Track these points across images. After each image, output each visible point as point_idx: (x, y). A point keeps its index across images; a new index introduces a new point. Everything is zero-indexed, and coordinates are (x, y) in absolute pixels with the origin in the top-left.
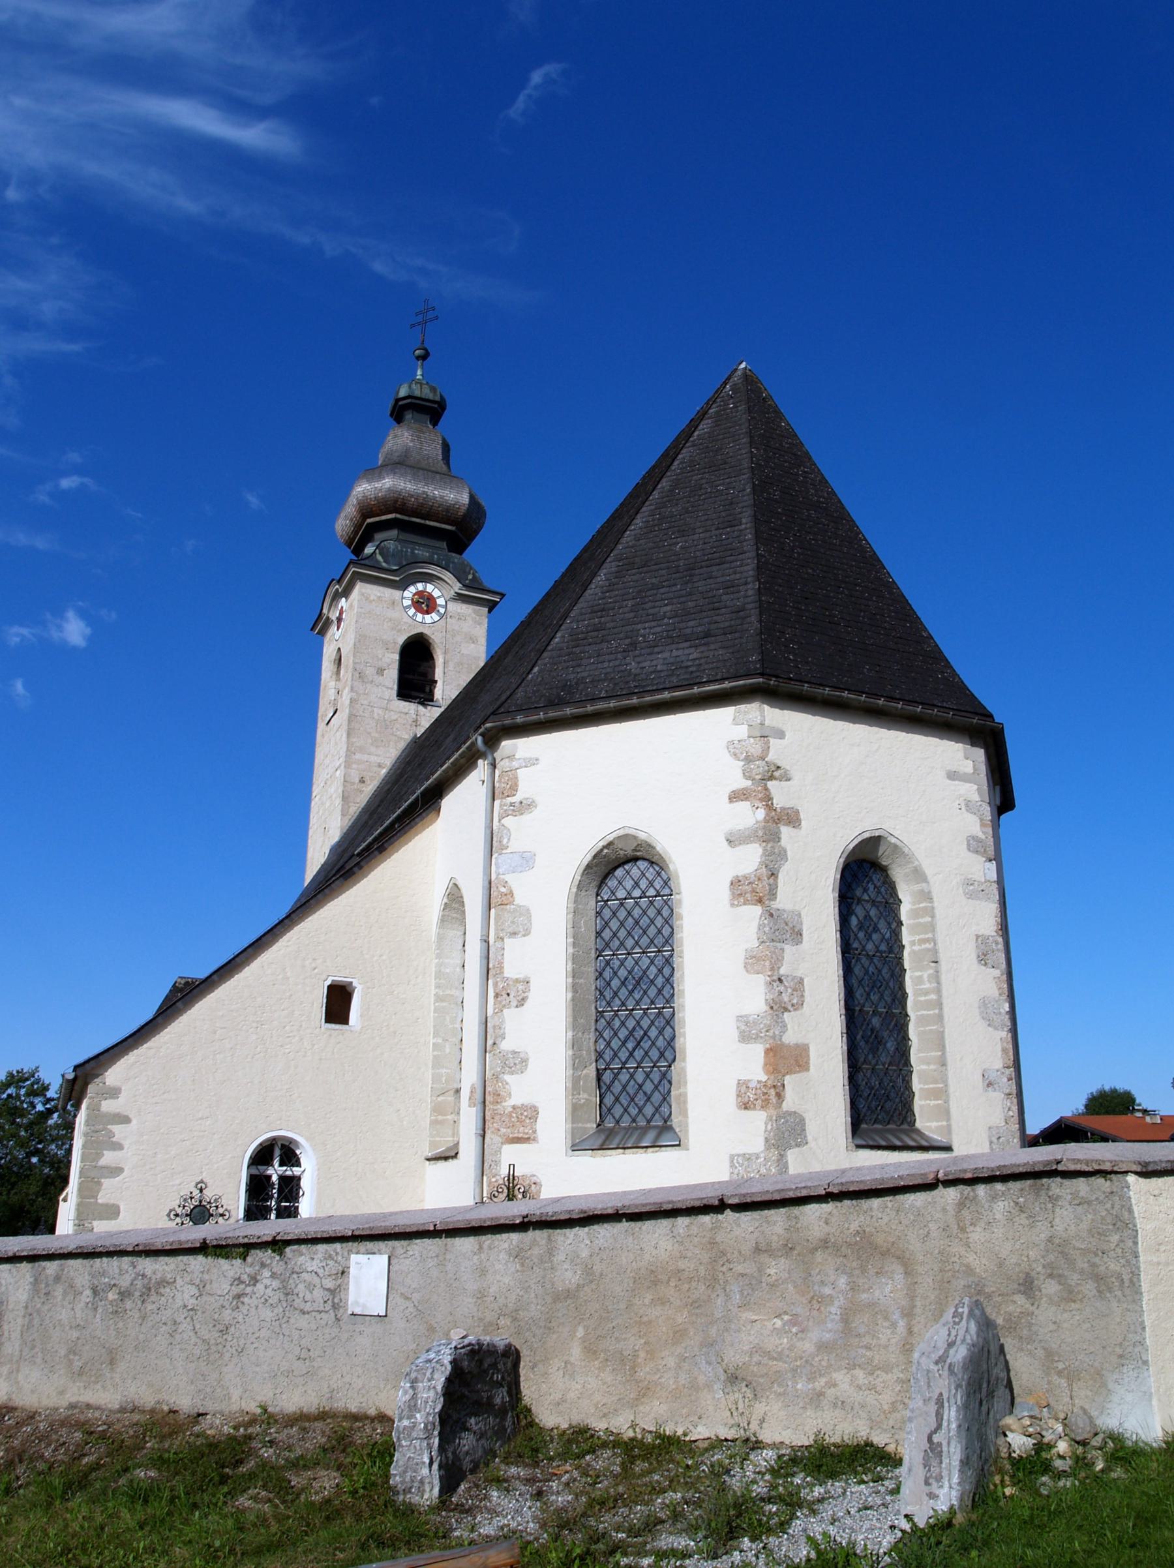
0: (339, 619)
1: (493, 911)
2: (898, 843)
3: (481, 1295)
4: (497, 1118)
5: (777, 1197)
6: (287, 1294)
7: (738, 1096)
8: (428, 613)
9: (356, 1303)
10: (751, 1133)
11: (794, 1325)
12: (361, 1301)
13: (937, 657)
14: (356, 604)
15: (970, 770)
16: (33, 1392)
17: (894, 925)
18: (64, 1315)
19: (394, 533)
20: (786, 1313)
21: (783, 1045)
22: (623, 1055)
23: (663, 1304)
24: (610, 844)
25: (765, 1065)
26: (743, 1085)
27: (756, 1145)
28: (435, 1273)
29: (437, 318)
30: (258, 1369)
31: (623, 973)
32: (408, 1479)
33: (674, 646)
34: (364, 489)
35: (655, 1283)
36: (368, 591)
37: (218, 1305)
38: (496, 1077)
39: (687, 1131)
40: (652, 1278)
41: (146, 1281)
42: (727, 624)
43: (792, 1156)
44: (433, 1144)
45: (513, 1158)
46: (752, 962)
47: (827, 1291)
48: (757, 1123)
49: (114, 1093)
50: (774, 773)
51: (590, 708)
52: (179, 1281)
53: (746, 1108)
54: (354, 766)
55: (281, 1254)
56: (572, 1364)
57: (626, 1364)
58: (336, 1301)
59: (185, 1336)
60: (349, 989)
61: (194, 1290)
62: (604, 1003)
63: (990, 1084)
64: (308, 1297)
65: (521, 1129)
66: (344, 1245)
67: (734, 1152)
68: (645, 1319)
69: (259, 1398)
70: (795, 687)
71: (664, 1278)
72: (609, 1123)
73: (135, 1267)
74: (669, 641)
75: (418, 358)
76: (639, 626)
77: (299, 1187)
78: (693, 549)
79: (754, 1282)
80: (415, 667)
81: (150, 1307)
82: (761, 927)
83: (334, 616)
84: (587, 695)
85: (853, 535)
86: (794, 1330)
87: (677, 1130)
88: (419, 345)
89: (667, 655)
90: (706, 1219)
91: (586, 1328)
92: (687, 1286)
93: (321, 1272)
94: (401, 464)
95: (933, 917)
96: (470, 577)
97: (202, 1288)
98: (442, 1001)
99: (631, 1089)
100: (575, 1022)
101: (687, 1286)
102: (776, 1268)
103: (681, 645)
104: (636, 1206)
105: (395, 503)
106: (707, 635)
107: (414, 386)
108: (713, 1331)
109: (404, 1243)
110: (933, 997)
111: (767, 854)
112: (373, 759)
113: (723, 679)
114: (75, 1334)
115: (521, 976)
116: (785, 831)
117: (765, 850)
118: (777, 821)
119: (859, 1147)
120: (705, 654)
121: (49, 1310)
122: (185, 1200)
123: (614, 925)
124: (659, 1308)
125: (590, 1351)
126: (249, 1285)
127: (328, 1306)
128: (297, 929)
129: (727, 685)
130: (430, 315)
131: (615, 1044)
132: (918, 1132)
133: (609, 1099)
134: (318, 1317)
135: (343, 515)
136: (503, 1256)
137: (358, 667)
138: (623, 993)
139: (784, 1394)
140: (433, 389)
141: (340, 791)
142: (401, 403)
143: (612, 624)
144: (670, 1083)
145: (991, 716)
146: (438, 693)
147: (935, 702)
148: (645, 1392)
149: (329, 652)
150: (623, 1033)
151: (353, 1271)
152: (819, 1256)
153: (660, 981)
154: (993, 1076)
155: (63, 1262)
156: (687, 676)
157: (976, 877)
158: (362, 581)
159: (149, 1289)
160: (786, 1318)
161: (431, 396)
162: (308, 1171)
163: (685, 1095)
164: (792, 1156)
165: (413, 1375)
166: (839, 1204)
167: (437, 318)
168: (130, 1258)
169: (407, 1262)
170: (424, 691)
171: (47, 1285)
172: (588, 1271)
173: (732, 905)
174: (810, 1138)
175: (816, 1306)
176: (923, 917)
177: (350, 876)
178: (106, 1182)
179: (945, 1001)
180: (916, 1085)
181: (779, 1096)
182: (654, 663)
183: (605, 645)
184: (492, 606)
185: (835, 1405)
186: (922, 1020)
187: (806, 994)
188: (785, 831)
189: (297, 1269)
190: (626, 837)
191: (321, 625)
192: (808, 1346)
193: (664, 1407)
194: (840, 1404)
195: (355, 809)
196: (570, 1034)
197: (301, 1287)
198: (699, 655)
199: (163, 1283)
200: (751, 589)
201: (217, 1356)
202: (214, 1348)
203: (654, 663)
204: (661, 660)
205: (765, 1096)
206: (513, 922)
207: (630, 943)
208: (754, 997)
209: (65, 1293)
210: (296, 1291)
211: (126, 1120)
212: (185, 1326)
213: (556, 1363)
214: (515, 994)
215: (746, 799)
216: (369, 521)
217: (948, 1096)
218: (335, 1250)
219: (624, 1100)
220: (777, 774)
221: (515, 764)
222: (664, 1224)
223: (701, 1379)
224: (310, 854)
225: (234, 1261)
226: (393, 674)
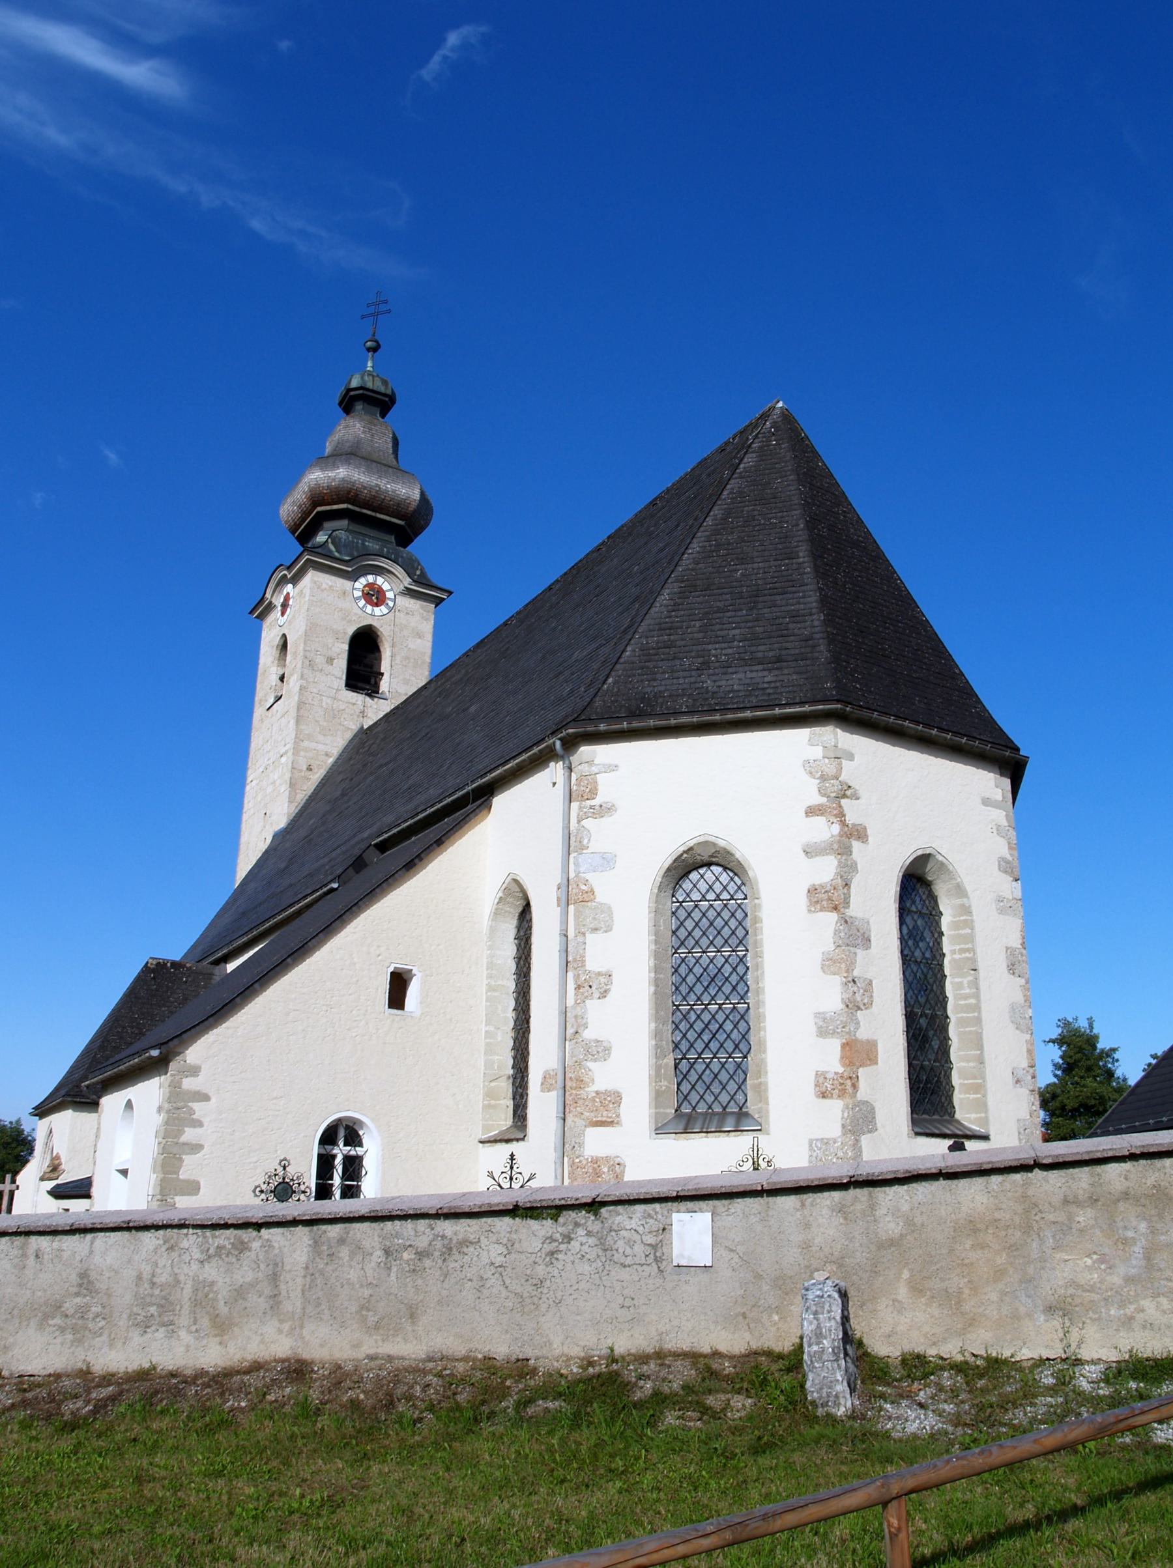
0: (285, 606)
1: (571, 907)
2: (944, 861)
3: (806, 1246)
4: (581, 1102)
5: (1087, 1157)
6: (606, 1250)
7: (816, 1085)
8: (377, 605)
9: (682, 1256)
10: (830, 1118)
11: (1102, 1263)
12: (686, 1254)
13: (968, 692)
14: (307, 592)
15: (999, 797)
16: (322, 1346)
17: (936, 935)
18: (353, 1275)
19: (344, 523)
20: (1095, 1253)
21: (856, 1040)
22: (699, 1046)
23: (982, 1248)
24: (691, 849)
25: (842, 1058)
26: (821, 1076)
27: (834, 1130)
28: (759, 1228)
29: (389, 311)
30: (578, 1318)
31: (698, 970)
32: (824, 1395)
33: (747, 668)
34: (316, 477)
35: (975, 1231)
36: (321, 579)
37: (531, 1261)
38: (579, 1063)
39: (767, 1118)
40: (971, 1227)
41: (446, 1242)
42: (797, 651)
43: (865, 1140)
44: (486, 1128)
45: (596, 1143)
46: (829, 964)
47: (1130, 1234)
48: (835, 1109)
49: (194, 1071)
50: (846, 792)
51: (673, 722)
52: (484, 1241)
53: (824, 1097)
54: (302, 753)
55: (596, 1215)
56: (899, 1302)
57: (952, 1300)
58: (658, 1254)
59: (494, 1290)
60: (405, 977)
61: (501, 1249)
62: (680, 998)
63: (1018, 1081)
64: (628, 1251)
65: (605, 1113)
66: (663, 1205)
67: (812, 1137)
68: (967, 1261)
69: (583, 1343)
70: (865, 714)
71: (983, 1227)
72: (686, 1109)
73: (433, 1229)
74: (742, 663)
75: (369, 350)
76: (710, 647)
77: (361, 1166)
78: (754, 577)
79: (1065, 1228)
80: (363, 659)
82: (836, 932)
83: (278, 601)
84: (667, 708)
85: (889, 575)
86: (1103, 1267)
87: (756, 1116)
88: (370, 337)
89: (741, 675)
90: (1017, 1177)
91: (911, 1270)
92: (1004, 1233)
93: (640, 1229)
94: (350, 454)
95: (972, 929)
96: (418, 572)
97: (510, 1247)
98: (494, 990)
99: (707, 1077)
100: (657, 1017)
101: (1004, 1233)
102: (1084, 1217)
103: (754, 668)
104: (958, 1166)
106: (779, 660)
107: (366, 378)
108: (1031, 1270)
109: (726, 1202)
110: (973, 1001)
111: (841, 865)
112: (321, 747)
113: (802, 703)
114: (367, 1292)
115: (603, 970)
116: (856, 845)
117: (840, 862)
118: (849, 836)
119: (917, 1134)
120: (781, 678)
121: (335, 1270)
122: (270, 1177)
123: (689, 924)
124: (979, 1252)
125: (917, 1289)
126: (562, 1243)
127: (651, 1259)
128: (363, 917)
129: (807, 708)
130: (383, 307)
131: (691, 1035)
132: (958, 1122)
133: (685, 1087)
134: (640, 1269)
135: (290, 500)
136: (825, 1211)
137: (308, 654)
138: (699, 989)
139: (1099, 1319)
140: (385, 382)
141: (288, 776)
142: (352, 393)
143: (683, 643)
144: (745, 1074)
145: (1018, 750)
146: (384, 685)
147: (975, 735)
148: (972, 1322)
150: (699, 1026)
151: (675, 1228)
152: (1121, 1206)
153: (734, 979)
154: (1020, 1074)
155: (347, 1225)
156: (765, 698)
157: (1004, 895)
158: (315, 569)
159: (451, 1249)
160: (1095, 1257)
161: (382, 389)
162: (371, 1151)
163: (766, 1084)
164: (865, 1140)
165: (814, 1308)
166: (1135, 1163)
167: (389, 311)
168: (427, 1221)
169: (730, 1218)
170: (368, 682)
171: (330, 1247)
172: (909, 1222)
173: (810, 911)
174: (879, 1125)
175: (1121, 1246)
176: (963, 929)
177: (411, 867)
179: (983, 1006)
180: (956, 1080)
181: (854, 1086)
182: (730, 682)
183: (677, 662)
184: (438, 602)
185: (1144, 1327)
186: (962, 1022)
187: (874, 995)
188: (856, 845)
189: (615, 1227)
190: (706, 843)
191: (261, 609)
192: (1116, 1280)
193: (990, 1334)
194: (1147, 1326)
195: (302, 796)
196: (653, 1025)
197: (620, 1243)
198: (774, 679)
199: (466, 1242)
200: (818, 619)
201: (533, 1307)
202: (528, 1301)
203: (730, 682)
204: (736, 680)
205: (841, 1086)
206: (594, 919)
207: (704, 942)
208: (830, 996)
209: (352, 1255)
210: (616, 1247)
211: (206, 1098)
212: (493, 1281)
213: (883, 1304)
214: (595, 986)
215: (822, 815)
216: (319, 509)
217: (986, 1091)
218: (654, 1209)
219: (700, 1088)
220: (848, 793)
221: (594, 769)
222: (979, 1181)
223: (1022, 1310)
224: (244, 838)
225: (544, 1222)
226: (341, 664)
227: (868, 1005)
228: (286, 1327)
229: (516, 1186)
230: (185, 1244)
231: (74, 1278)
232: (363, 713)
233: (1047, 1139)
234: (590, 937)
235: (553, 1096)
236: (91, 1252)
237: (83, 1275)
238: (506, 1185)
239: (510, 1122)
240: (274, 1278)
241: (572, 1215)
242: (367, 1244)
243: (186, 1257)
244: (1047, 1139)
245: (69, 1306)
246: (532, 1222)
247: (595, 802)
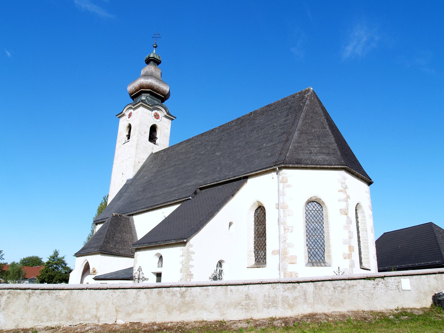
3: (429, 286)
18: (326, 293)
19: (148, 95)
26: (344, 254)
29: (160, 37)
45: (291, 268)
51: (308, 166)
52: (358, 285)
61: (362, 287)
75: (154, 47)
81: (351, 290)
83: (127, 114)
94: (146, 76)
97: (364, 286)
105: (150, 87)
113: (338, 165)
114: (330, 297)
116: (348, 199)
127: (397, 289)
129: (340, 166)
130: (158, 36)
149: (123, 123)
167: (160, 37)
170: (153, 140)
171: (319, 287)
184: (172, 119)
191: (121, 115)
200: (335, 145)
209: (325, 289)
228: (309, 306)
229: (340, 274)
230: (278, 287)
231: (244, 296)
233: (379, 271)
236: (249, 290)
237: (247, 295)
238: (338, 274)
240: (305, 295)
241: (378, 279)
242: (329, 286)
243: (279, 290)
244: (379, 271)
245: (243, 303)
246: (369, 281)
247: (288, 184)
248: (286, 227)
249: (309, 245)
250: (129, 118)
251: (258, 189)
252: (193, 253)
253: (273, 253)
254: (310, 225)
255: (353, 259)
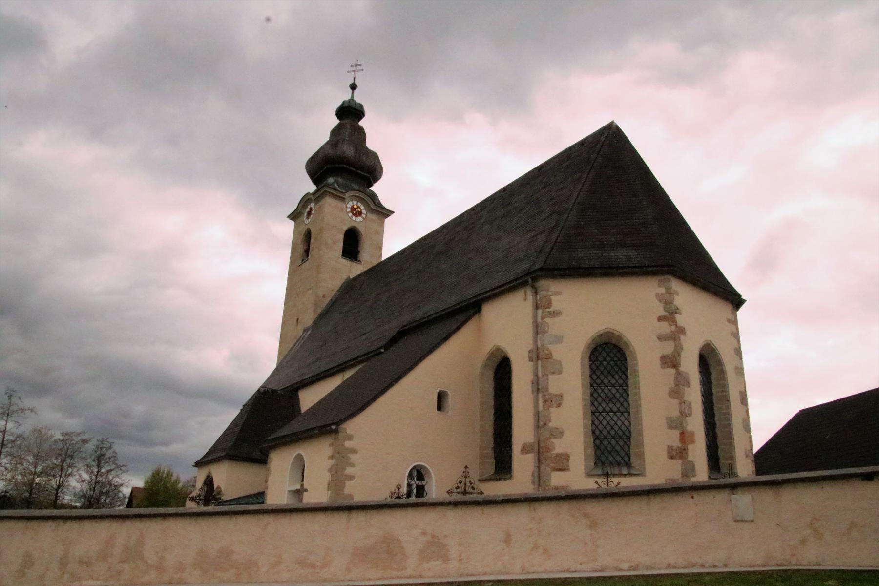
0: (309, 214)
26: (670, 448)
116: (682, 337)
178: (348, 483)
205: (679, 453)
214: (556, 400)
221: (550, 293)
226: (340, 246)
227: (690, 415)
232: (350, 272)
234: (551, 376)
235: (530, 458)
239: (493, 471)
247: (552, 309)
248: (547, 397)
249: (597, 432)
250: (308, 218)
251: (506, 324)
252: (354, 451)
253: (525, 449)
254: (600, 391)
255: (690, 458)
